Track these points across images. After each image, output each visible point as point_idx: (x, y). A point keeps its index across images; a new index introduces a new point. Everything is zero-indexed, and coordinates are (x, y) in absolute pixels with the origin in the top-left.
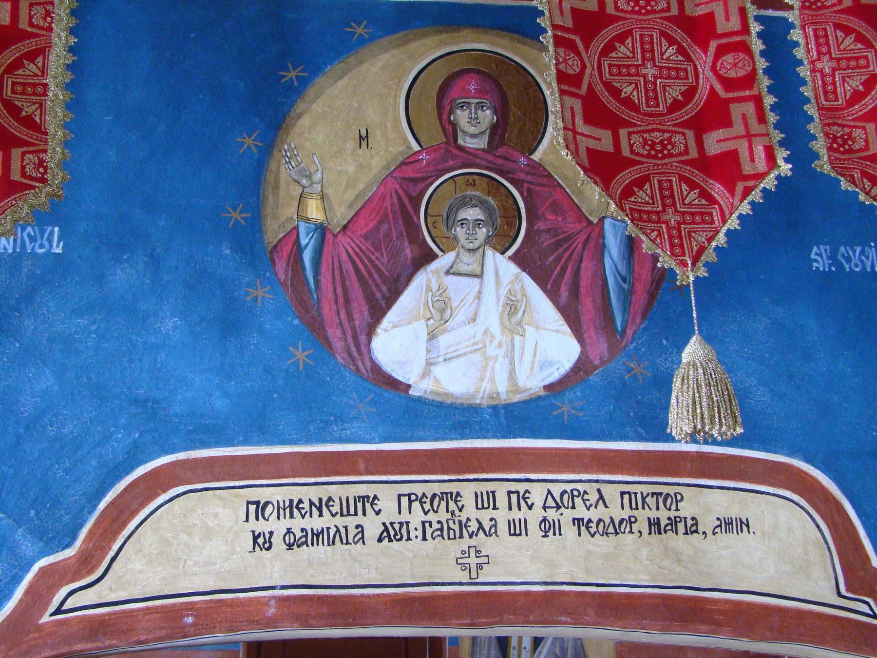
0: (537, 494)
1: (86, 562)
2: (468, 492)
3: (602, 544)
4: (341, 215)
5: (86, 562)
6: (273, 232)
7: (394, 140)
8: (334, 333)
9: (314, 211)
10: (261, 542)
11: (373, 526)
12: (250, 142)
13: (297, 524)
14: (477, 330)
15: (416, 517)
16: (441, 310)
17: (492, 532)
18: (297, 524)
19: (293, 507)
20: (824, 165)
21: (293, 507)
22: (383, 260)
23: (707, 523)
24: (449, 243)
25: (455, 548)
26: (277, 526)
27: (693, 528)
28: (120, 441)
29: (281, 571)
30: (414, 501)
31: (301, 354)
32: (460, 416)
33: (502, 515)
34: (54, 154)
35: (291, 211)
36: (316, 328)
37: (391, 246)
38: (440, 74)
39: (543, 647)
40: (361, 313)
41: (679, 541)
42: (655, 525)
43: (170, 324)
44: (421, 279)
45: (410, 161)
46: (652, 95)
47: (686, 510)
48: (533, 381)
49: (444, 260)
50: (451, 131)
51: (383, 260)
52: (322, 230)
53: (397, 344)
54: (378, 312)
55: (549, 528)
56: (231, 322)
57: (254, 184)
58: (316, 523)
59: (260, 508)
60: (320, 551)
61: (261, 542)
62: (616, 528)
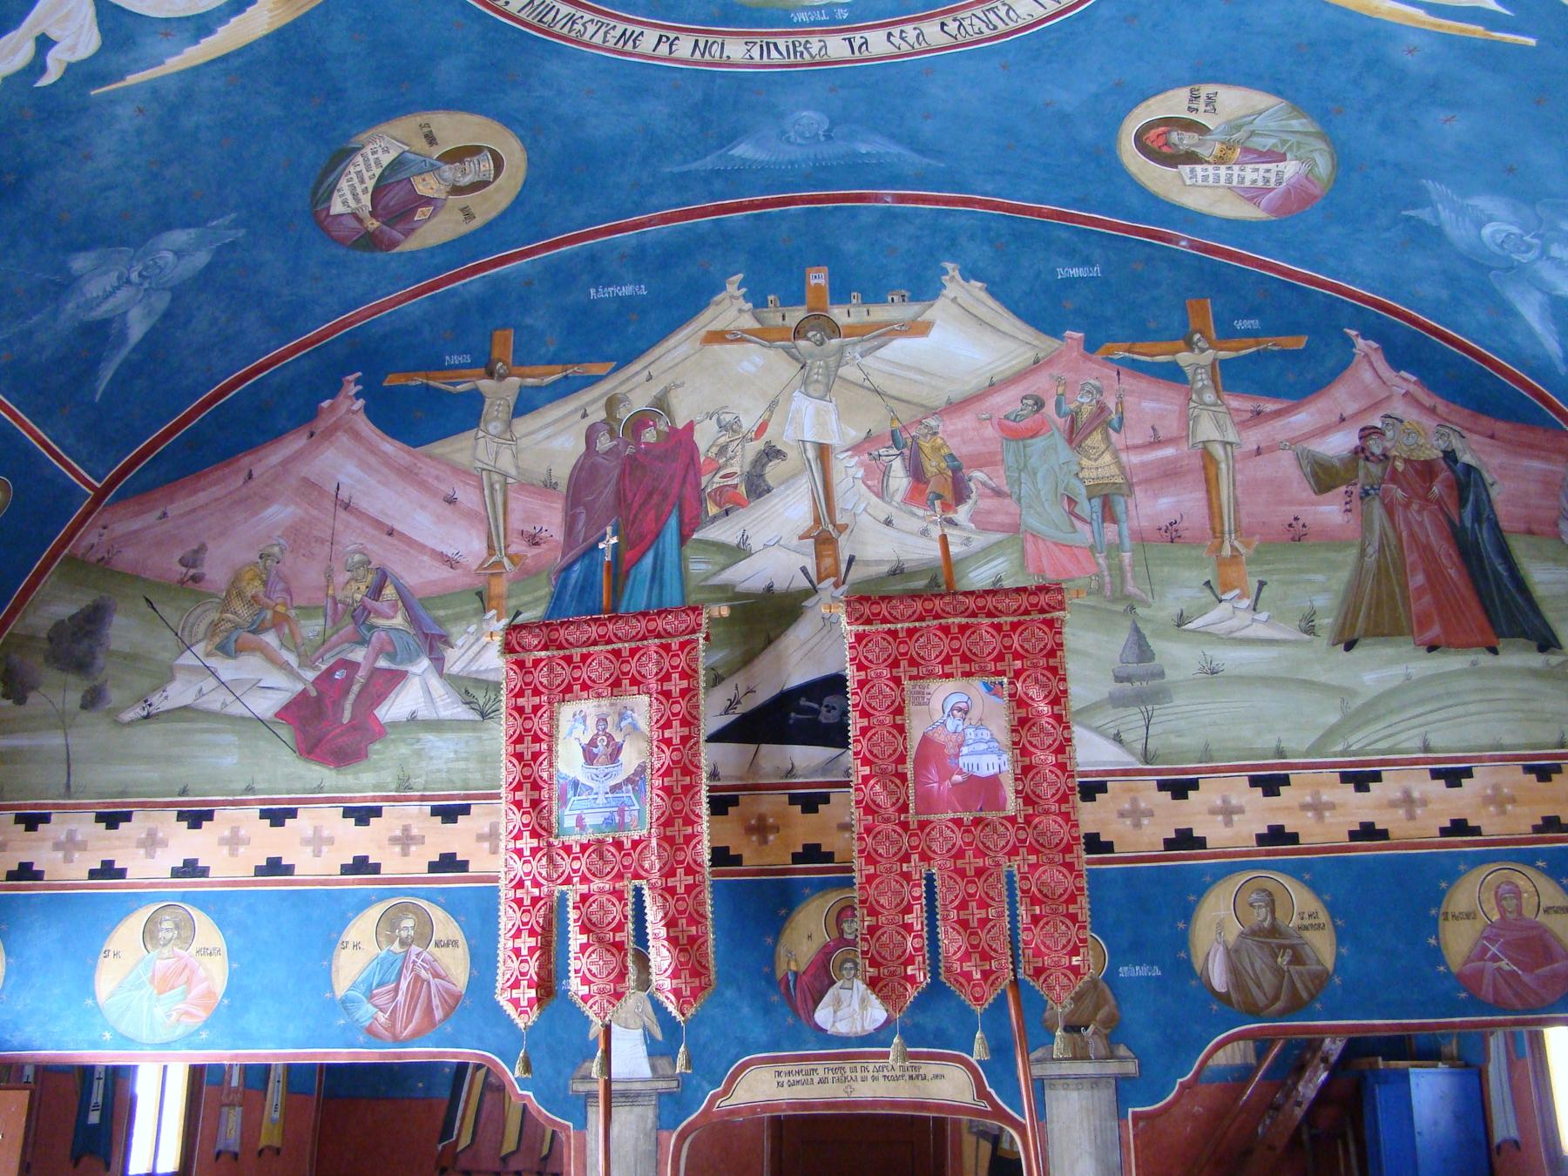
0: (871, 1067)
1: (725, 1092)
2: (847, 1066)
3: (893, 1084)
4: (803, 968)
5: (725, 1092)
6: (779, 974)
7: (822, 937)
8: (802, 1013)
9: (793, 967)
10: (780, 1085)
11: (816, 1079)
12: (769, 940)
13: (791, 1078)
14: (852, 1009)
15: (831, 1075)
16: (838, 1002)
17: (856, 1080)
18: (791, 1078)
19: (790, 1073)
20: (942, 978)
21: (790, 1073)
22: (817, 985)
23: (929, 1076)
24: (841, 977)
25: (843, 1086)
26: (784, 1079)
27: (924, 1078)
28: (733, 1051)
29: (786, 1094)
30: (1134, 801)
31: (790, 1020)
32: (844, 1040)
33: (859, 1074)
34: (713, 977)
35: (784, 967)
36: (795, 1011)
37: (820, 980)
38: (834, 913)
39: (312, 1154)
40: (810, 1002)
41: (919, 1083)
42: (911, 1077)
43: (746, 1010)
44: (831, 991)
45: (826, 946)
46: (892, 954)
47: (922, 1072)
48: (870, 1027)
49: (839, 983)
50: (841, 932)
51: (817, 985)
52: (796, 974)
53: (823, 1015)
54: (816, 1003)
55: (874, 1078)
56: (767, 1010)
57: (770, 958)
58: (798, 1078)
59: (779, 1073)
60: (799, 1087)
61: (780, 1085)
62: (897, 1078)
